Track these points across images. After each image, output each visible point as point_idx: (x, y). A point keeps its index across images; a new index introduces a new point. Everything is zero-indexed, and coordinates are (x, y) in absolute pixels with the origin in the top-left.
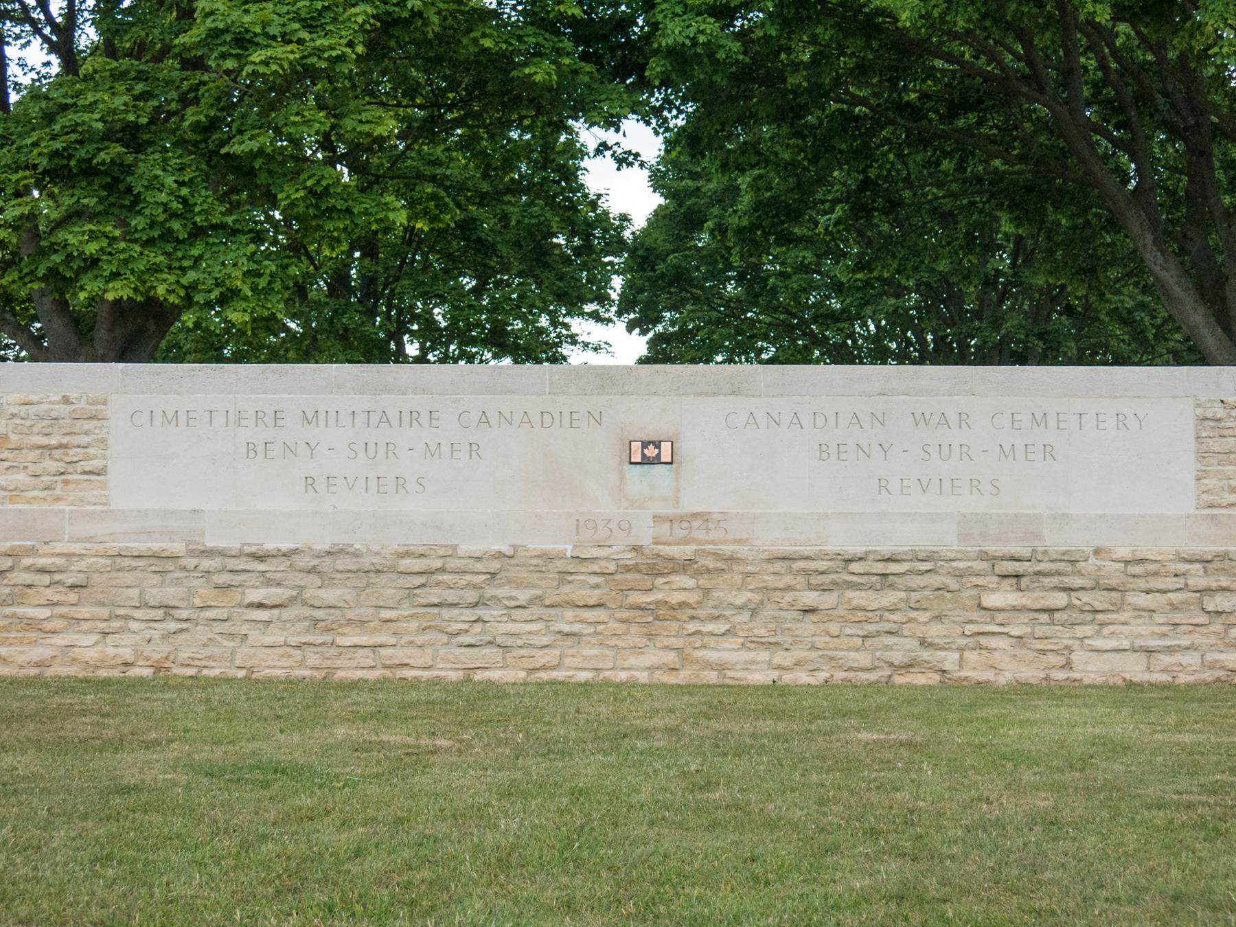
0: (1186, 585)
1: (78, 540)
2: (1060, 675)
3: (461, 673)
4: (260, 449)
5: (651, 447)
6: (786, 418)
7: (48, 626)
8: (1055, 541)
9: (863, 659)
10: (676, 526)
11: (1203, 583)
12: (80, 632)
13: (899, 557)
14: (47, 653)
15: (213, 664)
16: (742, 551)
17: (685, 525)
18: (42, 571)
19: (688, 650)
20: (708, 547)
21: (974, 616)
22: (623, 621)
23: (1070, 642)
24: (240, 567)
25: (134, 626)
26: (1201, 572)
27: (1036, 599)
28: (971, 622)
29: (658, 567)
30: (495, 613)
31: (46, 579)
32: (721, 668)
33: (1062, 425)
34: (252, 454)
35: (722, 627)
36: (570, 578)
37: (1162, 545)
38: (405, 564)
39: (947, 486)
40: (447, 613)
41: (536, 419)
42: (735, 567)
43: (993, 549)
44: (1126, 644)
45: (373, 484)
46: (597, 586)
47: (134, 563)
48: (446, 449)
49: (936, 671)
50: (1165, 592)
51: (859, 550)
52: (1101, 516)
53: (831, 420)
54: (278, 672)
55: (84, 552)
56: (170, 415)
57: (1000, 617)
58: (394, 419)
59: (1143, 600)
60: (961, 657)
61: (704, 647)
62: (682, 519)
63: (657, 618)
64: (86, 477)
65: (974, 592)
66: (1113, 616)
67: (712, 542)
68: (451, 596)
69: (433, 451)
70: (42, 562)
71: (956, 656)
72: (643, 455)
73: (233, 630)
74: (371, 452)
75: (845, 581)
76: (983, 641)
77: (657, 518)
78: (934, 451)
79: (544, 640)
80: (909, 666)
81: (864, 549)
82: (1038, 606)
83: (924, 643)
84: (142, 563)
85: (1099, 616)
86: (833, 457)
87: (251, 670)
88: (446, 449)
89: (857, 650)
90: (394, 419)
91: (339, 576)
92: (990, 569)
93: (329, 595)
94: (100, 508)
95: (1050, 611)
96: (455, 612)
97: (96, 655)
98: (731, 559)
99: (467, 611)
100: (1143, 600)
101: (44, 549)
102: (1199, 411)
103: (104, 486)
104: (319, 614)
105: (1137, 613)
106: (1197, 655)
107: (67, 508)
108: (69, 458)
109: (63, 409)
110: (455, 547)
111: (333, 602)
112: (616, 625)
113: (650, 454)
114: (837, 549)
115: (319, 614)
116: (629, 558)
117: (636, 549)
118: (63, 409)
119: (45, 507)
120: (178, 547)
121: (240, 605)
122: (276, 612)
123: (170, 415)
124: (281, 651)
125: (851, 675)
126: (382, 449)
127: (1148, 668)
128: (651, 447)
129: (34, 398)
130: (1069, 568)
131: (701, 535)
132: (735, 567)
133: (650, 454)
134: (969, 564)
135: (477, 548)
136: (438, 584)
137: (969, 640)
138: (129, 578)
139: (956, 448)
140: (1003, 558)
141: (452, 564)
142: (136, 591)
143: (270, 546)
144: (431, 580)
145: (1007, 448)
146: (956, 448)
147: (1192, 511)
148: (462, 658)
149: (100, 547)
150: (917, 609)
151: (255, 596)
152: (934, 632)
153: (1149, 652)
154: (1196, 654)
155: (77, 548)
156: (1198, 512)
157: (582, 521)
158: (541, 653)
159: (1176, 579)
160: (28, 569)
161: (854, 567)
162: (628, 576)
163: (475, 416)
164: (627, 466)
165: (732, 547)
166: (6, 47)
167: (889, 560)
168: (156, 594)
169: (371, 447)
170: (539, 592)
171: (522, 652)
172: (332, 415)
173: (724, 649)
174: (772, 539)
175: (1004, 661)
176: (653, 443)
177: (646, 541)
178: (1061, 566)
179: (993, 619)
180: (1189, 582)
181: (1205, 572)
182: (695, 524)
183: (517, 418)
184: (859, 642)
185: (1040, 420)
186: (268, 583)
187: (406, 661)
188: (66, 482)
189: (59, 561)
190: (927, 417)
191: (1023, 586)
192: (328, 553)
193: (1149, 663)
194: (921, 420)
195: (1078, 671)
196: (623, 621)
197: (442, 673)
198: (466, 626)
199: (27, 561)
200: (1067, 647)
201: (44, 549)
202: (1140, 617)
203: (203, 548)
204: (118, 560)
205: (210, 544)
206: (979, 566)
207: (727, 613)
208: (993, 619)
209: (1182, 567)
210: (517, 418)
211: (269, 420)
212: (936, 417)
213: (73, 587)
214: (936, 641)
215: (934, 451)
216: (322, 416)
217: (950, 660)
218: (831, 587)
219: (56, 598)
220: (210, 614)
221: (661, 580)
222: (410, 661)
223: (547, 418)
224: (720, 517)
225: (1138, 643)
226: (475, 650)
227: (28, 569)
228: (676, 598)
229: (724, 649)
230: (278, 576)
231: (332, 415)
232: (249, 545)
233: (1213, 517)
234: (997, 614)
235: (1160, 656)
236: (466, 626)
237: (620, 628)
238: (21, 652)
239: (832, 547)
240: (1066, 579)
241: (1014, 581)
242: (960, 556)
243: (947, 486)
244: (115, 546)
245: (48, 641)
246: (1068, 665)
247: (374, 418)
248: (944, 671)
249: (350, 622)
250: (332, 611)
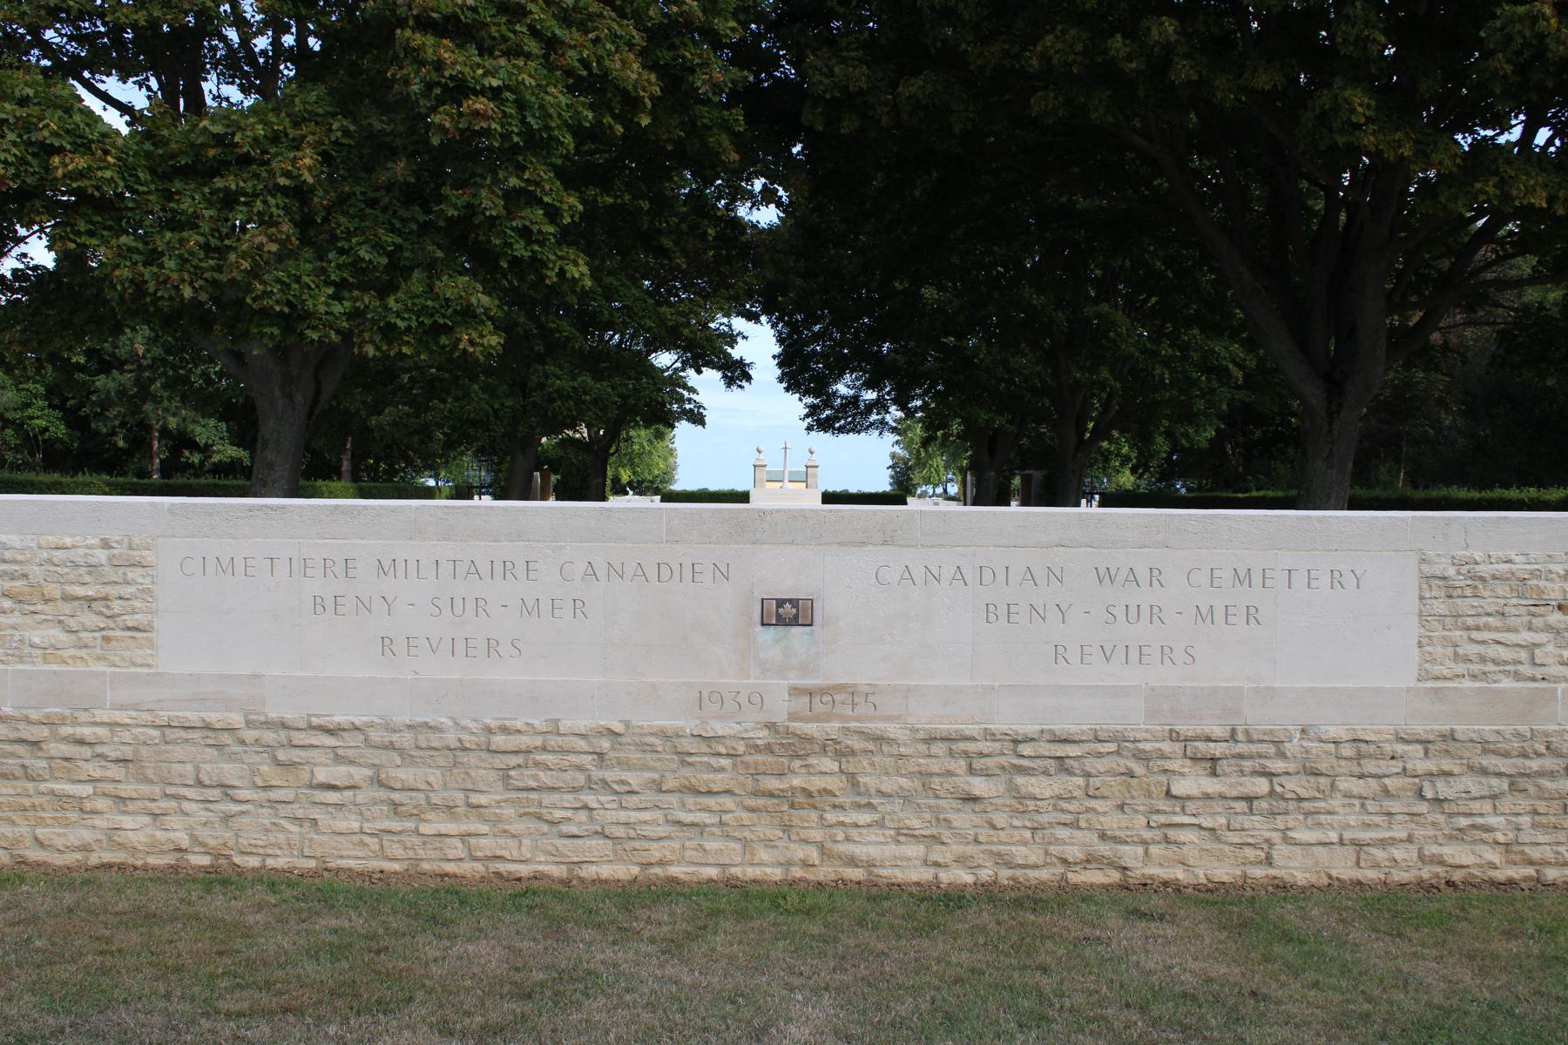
0: (1404, 769)
1: (122, 708)
2: (1258, 872)
3: (564, 867)
4: (329, 604)
5: (788, 605)
6: (948, 573)
7: (88, 806)
8: (1257, 718)
9: (1035, 856)
10: (816, 699)
11: (1422, 766)
12: (125, 812)
13: (1077, 738)
14: (87, 836)
15: (278, 852)
16: (893, 730)
17: (826, 698)
18: (81, 742)
19: (828, 845)
20: (853, 725)
21: (1163, 805)
22: (752, 810)
23: (1267, 835)
24: (307, 742)
25: (186, 806)
26: (1422, 755)
27: (1231, 785)
28: (1158, 812)
29: (791, 746)
30: (602, 798)
31: (87, 751)
32: (870, 864)
33: (1269, 583)
34: (319, 609)
35: (864, 818)
36: (690, 759)
37: (1379, 726)
38: (499, 740)
39: (1134, 655)
40: (548, 799)
41: (652, 572)
42: (885, 748)
43: (1185, 729)
44: (1333, 836)
45: (460, 645)
46: (722, 769)
47: (183, 734)
48: (545, 607)
49: (1116, 868)
50: (1380, 777)
51: (1031, 729)
52: (1311, 690)
53: (1001, 576)
54: (352, 863)
55: (128, 721)
56: (225, 562)
57: (1191, 807)
58: (484, 569)
59: (1357, 786)
60: (1146, 852)
61: (848, 839)
62: (823, 691)
63: (792, 806)
64: (130, 634)
65: (1163, 778)
66: (1322, 804)
67: (858, 719)
68: (545, 778)
69: (529, 609)
70: (87, 732)
71: (1140, 850)
72: (778, 616)
73: (300, 813)
74: (458, 610)
75: (1014, 766)
76: (1171, 833)
77: (796, 691)
78: (1119, 612)
79: (661, 831)
80: (1089, 860)
81: (1038, 727)
82: (1235, 793)
83: (1103, 836)
84: (195, 735)
85: (1306, 804)
86: (1003, 618)
87: (322, 859)
88: (545, 607)
89: (1025, 844)
90: (484, 569)
91: (421, 753)
92: (1181, 752)
93: (405, 775)
94: (146, 670)
95: (1249, 799)
96: (555, 797)
97: (143, 840)
98: (880, 739)
99: (569, 797)
100: (1357, 786)
101: (83, 717)
102: (1426, 568)
103: (151, 644)
104: (396, 796)
105: (1347, 801)
106: (1413, 848)
107: (109, 670)
108: (107, 609)
109: (101, 556)
110: (556, 722)
111: (411, 783)
112: (745, 815)
113: (788, 613)
114: (1004, 728)
115: (396, 796)
116: (762, 737)
117: (771, 726)
118: (101, 556)
119: (81, 668)
120: (237, 719)
121: (311, 787)
122: (349, 794)
123: (225, 562)
124: (355, 838)
125: (1019, 873)
126: (471, 605)
127: (1358, 863)
128: (788, 605)
129: (68, 541)
130: (1272, 750)
131: (848, 711)
132: (885, 748)
133: (788, 613)
134: (1157, 745)
135: (583, 723)
136: (537, 764)
137: (1156, 832)
138: (178, 752)
139: (1145, 611)
140: (1196, 739)
141: (554, 741)
142: (189, 767)
143: (340, 719)
144: (516, 759)
145: (1204, 610)
146: (1145, 611)
147: (1413, 684)
148: (565, 850)
149: (147, 717)
150: (1095, 797)
151: (322, 775)
152: (1113, 822)
153: (1358, 845)
154: (1411, 847)
155: (120, 716)
156: (1420, 685)
157: (705, 695)
158: (655, 845)
159: (1393, 762)
160: (67, 740)
161: (1026, 749)
162: (760, 758)
163: (580, 568)
164: (759, 628)
165: (881, 725)
166: (683, 428)
167: (1066, 741)
168: (210, 772)
169: (459, 603)
170: (656, 776)
171: (637, 844)
172: (412, 565)
173: (870, 843)
174: (929, 715)
175: (1191, 854)
176: (790, 601)
177: (781, 718)
178: (1263, 748)
179: (1183, 808)
180: (1409, 766)
181: (1426, 754)
182: (838, 698)
183: (630, 570)
184: (1028, 834)
185: (1242, 578)
186: (339, 759)
187: (498, 853)
188: (107, 639)
189: (102, 732)
190: (1113, 573)
191: (1219, 771)
192: (410, 727)
193: (1358, 858)
194: (1106, 576)
195: (1280, 867)
196: (752, 810)
197: (540, 868)
198: (569, 814)
199: (66, 730)
200: (1267, 841)
201: (83, 717)
202: (1350, 805)
203: (262, 718)
204: (168, 731)
205: (274, 715)
206: (1166, 747)
207: (875, 801)
208: (1183, 808)
209: (1400, 748)
210: (630, 570)
211: (339, 569)
212: (1124, 572)
213: (117, 761)
214: (1118, 833)
215: (1119, 612)
216: (400, 566)
217: (1130, 854)
218: (997, 771)
219: (97, 774)
220: (274, 795)
221: (797, 763)
222: (504, 853)
223: (665, 571)
224: (868, 689)
225: (1347, 835)
226: (579, 842)
227: (67, 740)
228: (817, 783)
229: (870, 843)
230: (350, 752)
231: (412, 565)
232: (318, 716)
233: (1436, 691)
234: (1188, 803)
235: (1372, 850)
236: (569, 814)
237: (746, 817)
238: (59, 835)
239: (999, 727)
240: (1268, 763)
241: (1209, 764)
242: (1149, 736)
243: (1134, 655)
244: (163, 717)
245: (89, 822)
246: (1269, 861)
247: (462, 569)
248: (1125, 868)
249: (434, 807)
250: (413, 794)
